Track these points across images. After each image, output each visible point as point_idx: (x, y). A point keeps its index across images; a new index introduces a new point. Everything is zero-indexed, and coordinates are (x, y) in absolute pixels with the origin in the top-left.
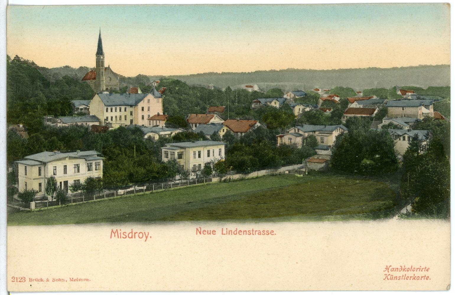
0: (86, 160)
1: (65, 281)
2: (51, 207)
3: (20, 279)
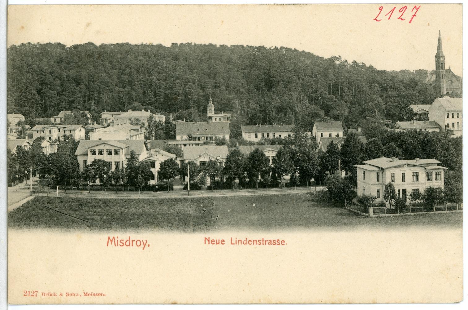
0: (425, 169)
1: (79, 295)
2: (390, 215)
3: (33, 293)
